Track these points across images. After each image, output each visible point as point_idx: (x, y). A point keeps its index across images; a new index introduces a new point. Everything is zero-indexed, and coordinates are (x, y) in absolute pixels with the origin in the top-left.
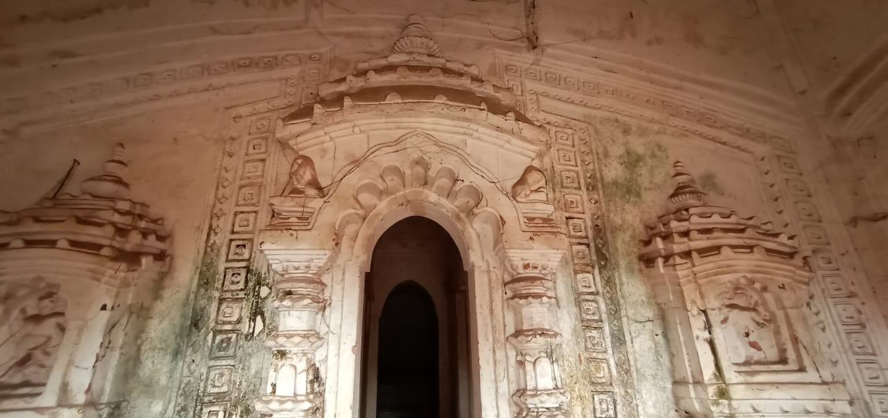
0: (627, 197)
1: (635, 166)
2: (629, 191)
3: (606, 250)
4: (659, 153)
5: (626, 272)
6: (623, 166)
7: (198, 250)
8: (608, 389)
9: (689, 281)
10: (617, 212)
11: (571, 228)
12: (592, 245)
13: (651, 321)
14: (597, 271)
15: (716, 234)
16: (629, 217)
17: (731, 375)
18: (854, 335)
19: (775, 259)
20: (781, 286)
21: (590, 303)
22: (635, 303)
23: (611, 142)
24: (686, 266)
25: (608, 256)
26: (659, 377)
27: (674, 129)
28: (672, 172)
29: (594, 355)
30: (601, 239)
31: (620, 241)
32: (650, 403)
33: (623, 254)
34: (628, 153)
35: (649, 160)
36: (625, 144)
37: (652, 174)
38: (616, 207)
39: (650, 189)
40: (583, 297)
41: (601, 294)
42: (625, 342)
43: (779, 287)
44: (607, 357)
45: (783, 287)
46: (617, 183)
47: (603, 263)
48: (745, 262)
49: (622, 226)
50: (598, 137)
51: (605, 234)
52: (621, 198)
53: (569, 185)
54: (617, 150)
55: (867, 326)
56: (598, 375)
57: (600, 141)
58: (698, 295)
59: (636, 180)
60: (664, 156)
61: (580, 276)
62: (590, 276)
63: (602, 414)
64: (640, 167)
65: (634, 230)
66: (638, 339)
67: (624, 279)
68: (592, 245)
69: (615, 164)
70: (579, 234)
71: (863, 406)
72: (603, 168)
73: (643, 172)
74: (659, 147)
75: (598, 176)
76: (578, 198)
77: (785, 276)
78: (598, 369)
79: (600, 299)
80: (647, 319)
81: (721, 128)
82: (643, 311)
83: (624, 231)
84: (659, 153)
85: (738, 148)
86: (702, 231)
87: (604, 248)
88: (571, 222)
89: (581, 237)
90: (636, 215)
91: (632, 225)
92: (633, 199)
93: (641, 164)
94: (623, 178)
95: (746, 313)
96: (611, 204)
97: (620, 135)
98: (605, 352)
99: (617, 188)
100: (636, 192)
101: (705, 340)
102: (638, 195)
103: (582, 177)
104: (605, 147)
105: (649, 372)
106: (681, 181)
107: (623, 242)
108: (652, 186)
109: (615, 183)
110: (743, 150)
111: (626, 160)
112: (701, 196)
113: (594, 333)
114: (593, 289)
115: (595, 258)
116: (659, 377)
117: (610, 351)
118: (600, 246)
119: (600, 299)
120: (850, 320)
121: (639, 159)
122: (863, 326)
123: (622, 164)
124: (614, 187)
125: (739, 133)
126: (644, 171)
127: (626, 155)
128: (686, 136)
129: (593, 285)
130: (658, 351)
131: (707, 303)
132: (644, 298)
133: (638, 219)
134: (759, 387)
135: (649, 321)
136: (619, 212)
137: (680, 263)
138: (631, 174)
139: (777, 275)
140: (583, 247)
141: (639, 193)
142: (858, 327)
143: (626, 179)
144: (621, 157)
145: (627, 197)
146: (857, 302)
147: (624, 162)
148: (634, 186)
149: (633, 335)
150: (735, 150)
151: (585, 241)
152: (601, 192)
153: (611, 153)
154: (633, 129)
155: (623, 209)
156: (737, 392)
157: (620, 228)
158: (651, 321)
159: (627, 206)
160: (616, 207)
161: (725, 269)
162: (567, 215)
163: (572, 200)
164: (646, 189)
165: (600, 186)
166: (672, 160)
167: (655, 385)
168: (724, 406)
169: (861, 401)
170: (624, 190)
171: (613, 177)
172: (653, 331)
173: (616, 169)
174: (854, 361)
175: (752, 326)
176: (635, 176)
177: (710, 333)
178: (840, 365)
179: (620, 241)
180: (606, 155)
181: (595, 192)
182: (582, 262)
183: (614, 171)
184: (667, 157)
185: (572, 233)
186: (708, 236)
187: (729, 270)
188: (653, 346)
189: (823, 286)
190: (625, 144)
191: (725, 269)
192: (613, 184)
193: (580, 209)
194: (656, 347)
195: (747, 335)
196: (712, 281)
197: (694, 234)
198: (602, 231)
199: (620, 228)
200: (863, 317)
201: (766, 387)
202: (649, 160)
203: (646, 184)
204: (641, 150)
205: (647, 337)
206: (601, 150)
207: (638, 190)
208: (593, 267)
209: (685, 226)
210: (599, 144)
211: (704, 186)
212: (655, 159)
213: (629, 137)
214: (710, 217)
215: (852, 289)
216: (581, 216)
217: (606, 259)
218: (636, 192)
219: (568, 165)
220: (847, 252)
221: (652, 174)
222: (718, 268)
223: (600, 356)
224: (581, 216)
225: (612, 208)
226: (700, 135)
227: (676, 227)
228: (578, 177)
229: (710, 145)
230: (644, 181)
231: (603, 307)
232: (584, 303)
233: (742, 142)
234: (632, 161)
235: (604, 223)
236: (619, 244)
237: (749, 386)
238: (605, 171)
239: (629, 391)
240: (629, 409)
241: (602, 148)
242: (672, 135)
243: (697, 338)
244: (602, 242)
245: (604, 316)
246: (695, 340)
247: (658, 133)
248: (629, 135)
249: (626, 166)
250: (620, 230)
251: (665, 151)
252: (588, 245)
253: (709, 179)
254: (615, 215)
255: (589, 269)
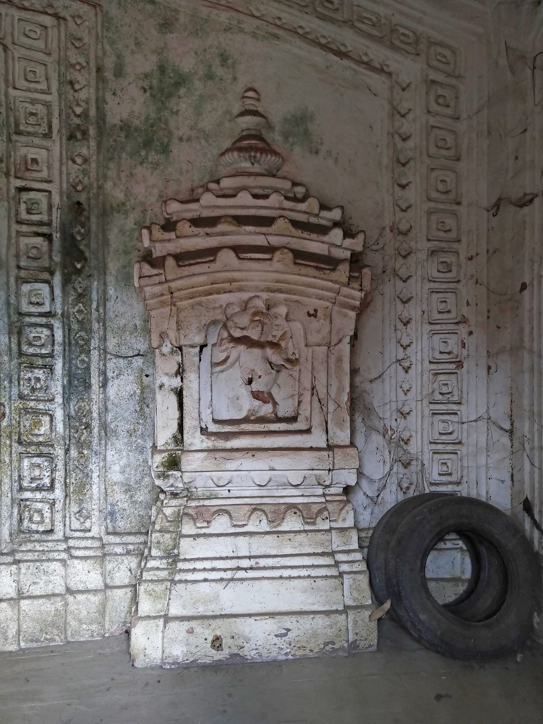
0: (143, 153)
1: (170, 96)
2: (147, 144)
3: (86, 245)
4: (219, 71)
5: (117, 280)
6: (148, 94)
7: (421, 155)
8: (45, 450)
9: (163, 304)
10: (120, 179)
11: (23, 207)
12: (57, 236)
13: (142, 355)
14: (57, 280)
15: (221, 227)
16: (139, 190)
17: (194, 439)
18: (441, 377)
19: (304, 270)
20: (312, 312)
21: (39, 329)
22: (123, 329)
23: (132, 46)
24: (157, 279)
25: (87, 254)
26: (139, 433)
27: (258, 22)
28: (236, 109)
29: (32, 404)
30: (83, 226)
31: (116, 230)
32: (117, 468)
33: (117, 251)
34: (162, 69)
35: (198, 84)
36: (160, 51)
37: (198, 112)
38: (119, 171)
39: (189, 139)
40: (27, 319)
41: (59, 316)
42: (88, 386)
43: (309, 315)
44: (51, 407)
45: (314, 315)
46: (130, 127)
47: (79, 266)
48: (258, 274)
49: (123, 204)
50: (110, 34)
51: (88, 218)
52: (132, 155)
53: (30, 129)
54: (142, 63)
55: (465, 365)
56: (36, 432)
57: (112, 43)
58: (174, 326)
59: (166, 123)
60: (230, 76)
61: (26, 288)
62: (45, 289)
63: (31, 483)
64: (180, 97)
65: (144, 211)
66: (116, 381)
67: (111, 292)
68: (57, 236)
69: (134, 91)
70: (35, 218)
71: (419, 468)
72: (109, 97)
73: (183, 106)
74: (224, 58)
75: (93, 112)
76: (44, 153)
77: (321, 298)
78: (38, 424)
79: (57, 324)
80: (136, 352)
81: (347, 23)
82: (133, 341)
83: (126, 213)
84: (219, 71)
85: (368, 65)
86: (196, 222)
87: (84, 242)
88: (25, 196)
89: (41, 224)
90: (154, 186)
91: (143, 204)
92: (153, 157)
93: (182, 91)
94: (143, 118)
95: (257, 351)
96: (112, 165)
97: (154, 32)
98: (52, 400)
99: (127, 137)
100: (162, 144)
101: (172, 390)
102: (165, 150)
103: (56, 114)
104: (119, 56)
105: (123, 427)
106: (244, 126)
107: (122, 231)
108: (193, 134)
109: (126, 127)
110: (373, 69)
111: (155, 82)
112: (255, 157)
113: (39, 373)
114: (46, 309)
115: (57, 258)
116: (139, 433)
117: (59, 399)
118: (79, 238)
119: (57, 324)
120: (446, 356)
121: (181, 81)
122: (460, 364)
123: (145, 91)
124: (123, 135)
125: (375, 32)
126: (183, 105)
127: (157, 74)
128: (277, 37)
129: (47, 302)
130: (144, 399)
131: (182, 337)
132: (138, 322)
133: (156, 192)
134: (223, 454)
135: (138, 355)
136: (124, 180)
137: (149, 274)
138: (159, 110)
139: (308, 296)
140: (39, 240)
141: (167, 145)
142: (453, 366)
143: (147, 119)
144: (146, 76)
145: (143, 153)
146: (463, 330)
147: (151, 88)
148: (161, 133)
149: (110, 374)
150: (361, 69)
151: (44, 230)
152: (93, 143)
153: (128, 69)
154: (183, 19)
155: (132, 175)
156: (191, 462)
157: (121, 208)
158: (142, 355)
159: (139, 170)
160: (119, 171)
161: (226, 286)
162: (20, 183)
163: (33, 156)
164: (181, 139)
165: (92, 131)
166: (242, 83)
167: (129, 444)
168: (177, 479)
169: (420, 461)
170: (140, 140)
171: (125, 116)
172: (142, 370)
173: (133, 100)
174: (427, 412)
175: (261, 368)
176: (166, 113)
177: (182, 381)
178: (411, 418)
179: (116, 230)
180: (119, 72)
181: (86, 143)
182: (35, 264)
183: (128, 104)
184: (235, 79)
185: (24, 216)
186: (208, 230)
187: (232, 286)
188: (138, 391)
189: (425, 307)
190: (160, 51)
191: (226, 286)
192: (121, 129)
193: (44, 174)
194: (142, 392)
195: (250, 382)
196: (200, 304)
197: (185, 228)
198: (86, 213)
199: (121, 208)
200: (465, 352)
201: (237, 454)
202: (198, 84)
203: (184, 131)
204: (187, 64)
205: (131, 378)
206: (109, 63)
207: (166, 140)
208: (52, 273)
209: (195, 210)
210: (107, 47)
211: (286, 136)
212: (210, 83)
213: (169, 36)
214: (234, 196)
215: (465, 311)
216: (44, 186)
217: (86, 259)
218: (162, 144)
219: (36, 91)
220: (477, 254)
221: (198, 112)
222: (212, 284)
223: (41, 406)
224: (44, 186)
225: (112, 174)
226: (304, 37)
227: (176, 212)
228: (50, 115)
229: (319, 57)
230: (180, 125)
231: (59, 335)
232: (28, 330)
233: (377, 53)
234: (166, 85)
235: (89, 199)
236: (113, 235)
237: (212, 455)
238: (111, 101)
239: (85, 452)
240: (80, 476)
241: (113, 58)
242: (254, 35)
243: (161, 387)
244: (82, 231)
245: (58, 349)
246: (157, 390)
247: (228, 29)
248: (171, 32)
249: (152, 95)
250: (119, 212)
251: (233, 66)
252: (48, 237)
253: (300, 125)
254: (115, 185)
255: (46, 276)
